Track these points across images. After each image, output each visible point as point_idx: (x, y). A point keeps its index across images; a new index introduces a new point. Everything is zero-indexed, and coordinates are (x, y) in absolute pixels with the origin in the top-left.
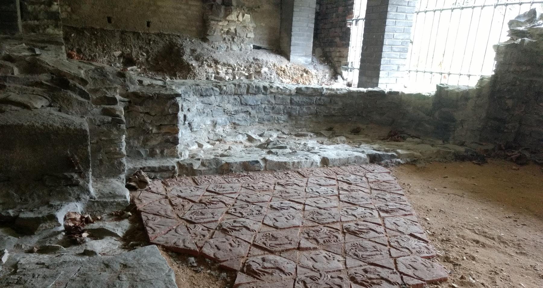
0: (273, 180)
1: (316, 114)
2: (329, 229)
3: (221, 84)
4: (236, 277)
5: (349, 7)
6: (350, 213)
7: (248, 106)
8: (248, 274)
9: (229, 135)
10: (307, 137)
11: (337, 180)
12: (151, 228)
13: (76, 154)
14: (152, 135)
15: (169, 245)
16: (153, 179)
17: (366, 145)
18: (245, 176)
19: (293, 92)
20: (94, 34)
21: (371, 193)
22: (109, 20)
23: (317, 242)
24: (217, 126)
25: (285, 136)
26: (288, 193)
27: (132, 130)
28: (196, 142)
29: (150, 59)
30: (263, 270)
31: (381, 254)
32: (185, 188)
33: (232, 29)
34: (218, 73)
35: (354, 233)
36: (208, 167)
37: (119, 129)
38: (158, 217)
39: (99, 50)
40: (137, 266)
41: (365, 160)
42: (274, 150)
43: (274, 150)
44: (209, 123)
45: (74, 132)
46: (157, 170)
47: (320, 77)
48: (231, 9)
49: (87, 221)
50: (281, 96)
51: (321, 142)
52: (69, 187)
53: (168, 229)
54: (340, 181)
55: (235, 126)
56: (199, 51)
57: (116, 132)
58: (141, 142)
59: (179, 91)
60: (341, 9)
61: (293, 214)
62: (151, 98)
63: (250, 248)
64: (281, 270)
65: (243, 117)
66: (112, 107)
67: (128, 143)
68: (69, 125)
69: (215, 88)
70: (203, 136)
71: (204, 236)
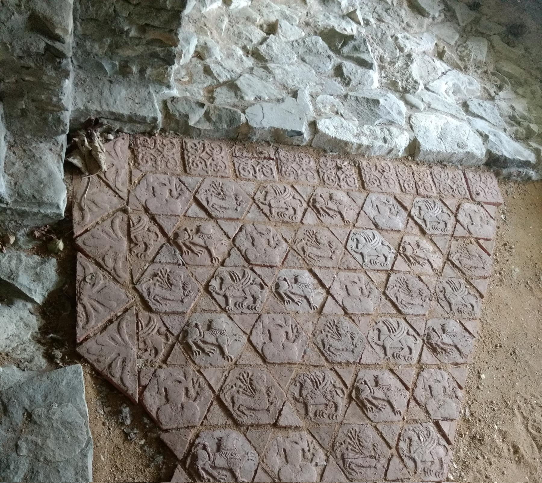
12: (84, 307)
27: (90, 26)
36: (214, 124)
37: (58, 68)
40: (45, 423)
57: (52, 73)
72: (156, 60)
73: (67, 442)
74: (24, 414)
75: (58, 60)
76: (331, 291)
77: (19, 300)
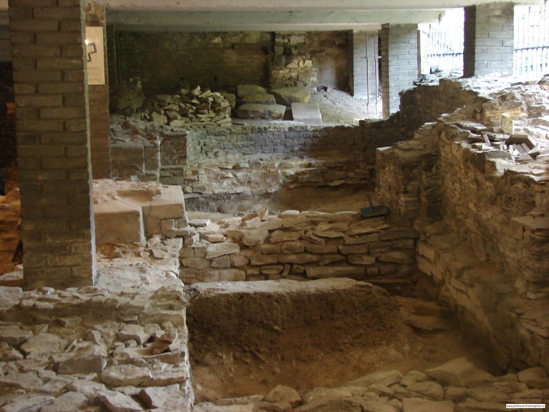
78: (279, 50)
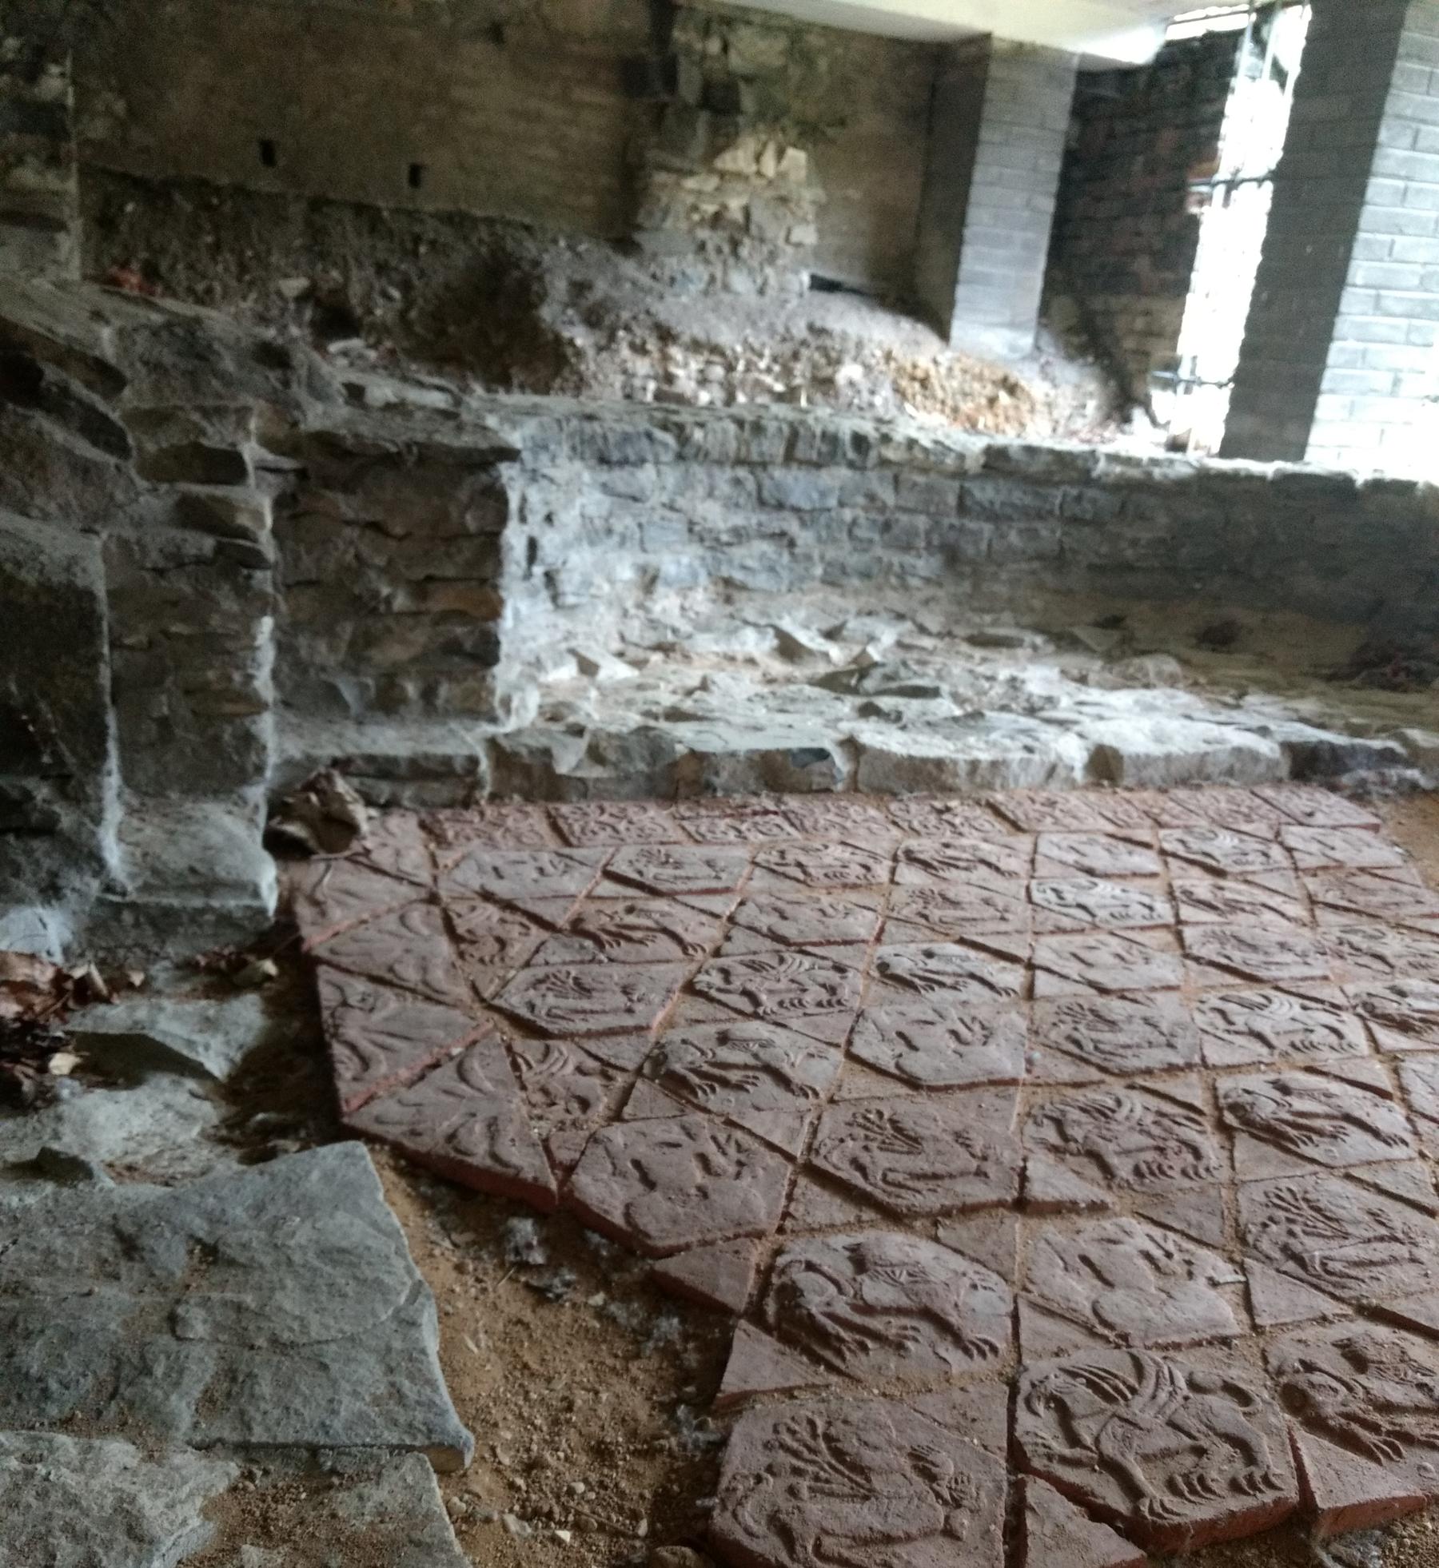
0: (887, 839)
1: (1059, 560)
2: (1154, 1103)
3: (685, 417)
4: (726, 1347)
5: (1204, 131)
6: (1240, 1025)
7: (786, 514)
8: (787, 1339)
9: (706, 627)
10: (1020, 652)
11: (1163, 852)
12: (353, 1047)
13: (45, 695)
14: (390, 622)
15: (423, 1145)
16: (388, 807)
17: (1269, 699)
18: (766, 812)
19: (973, 465)
20: (208, 207)
21: (1314, 923)
22: (268, 152)
23: (1107, 1170)
24: (660, 589)
25: (927, 642)
26: (955, 904)
27: (306, 598)
28: (573, 652)
29: (413, 314)
30: (858, 1319)
31: (1413, 1260)
32: (514, 855)
33: (735, 205)
34: (669, 378)
35: (1272, 1135)
36: (615, 765)
37: (243, 591)
38: (387, 993)
39: (226, 269)
40: (267, 1260)
41: (1272, 764)
42: (885, 703)
43: (885, 703)
44: (626, 573)
45: (36, 596)
46: (403, 770)
47: (1063, 410)
48: (736, 125)
49: (84, 993)
50: (921, 479)
51: (1075, 672)
52: (11, 838)
53: (428, 1060)
54: (1175, 855)
55: (729, 589)
56: (601, 287)
57: (230, 604)
58: (343, 647)
59: (515, 438)
60: (1168, 138)
61: (983, 1014)
62: (390, 460)
63: (793, 1184)
64: (944, 1327)
65: (763, 556)
66: (220, 491)
67: (283, 648)
68: (19, 565)
69: (659, 434)
70: (600, 630)
71: (585, 1104)
72: (456, 659)
73: (344, 1296)
74: (191, 1252)
75: (245, 572)
76: (1037, 961)
77: (159, 1075)
78: (689, 87)
